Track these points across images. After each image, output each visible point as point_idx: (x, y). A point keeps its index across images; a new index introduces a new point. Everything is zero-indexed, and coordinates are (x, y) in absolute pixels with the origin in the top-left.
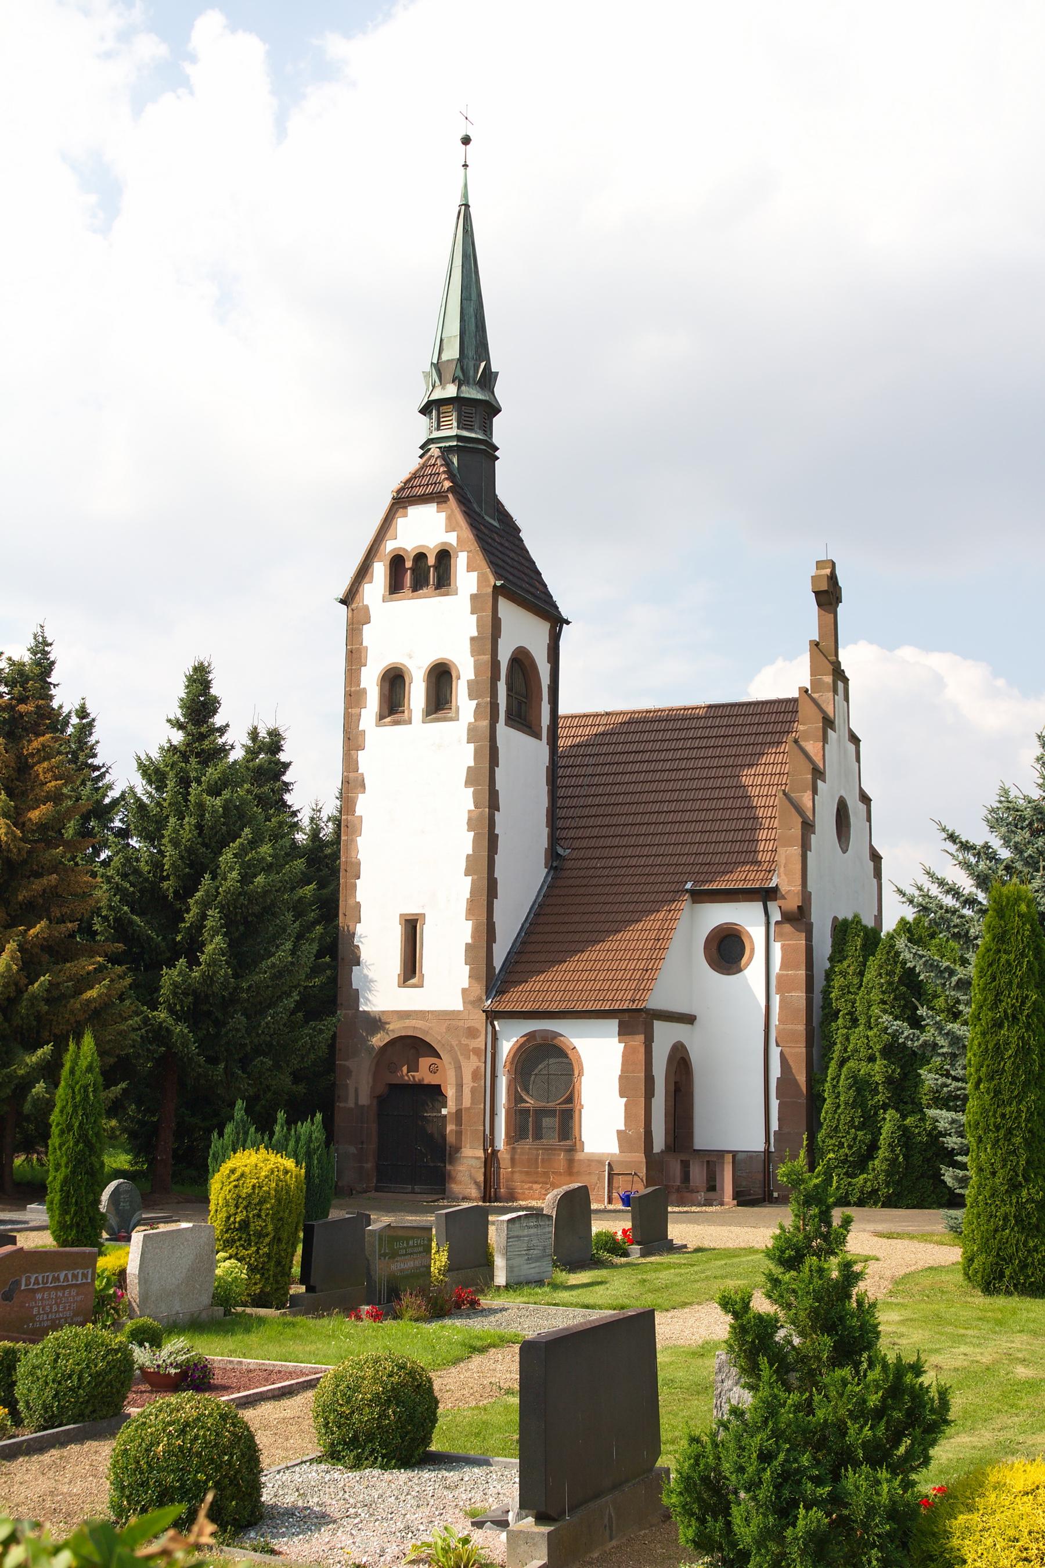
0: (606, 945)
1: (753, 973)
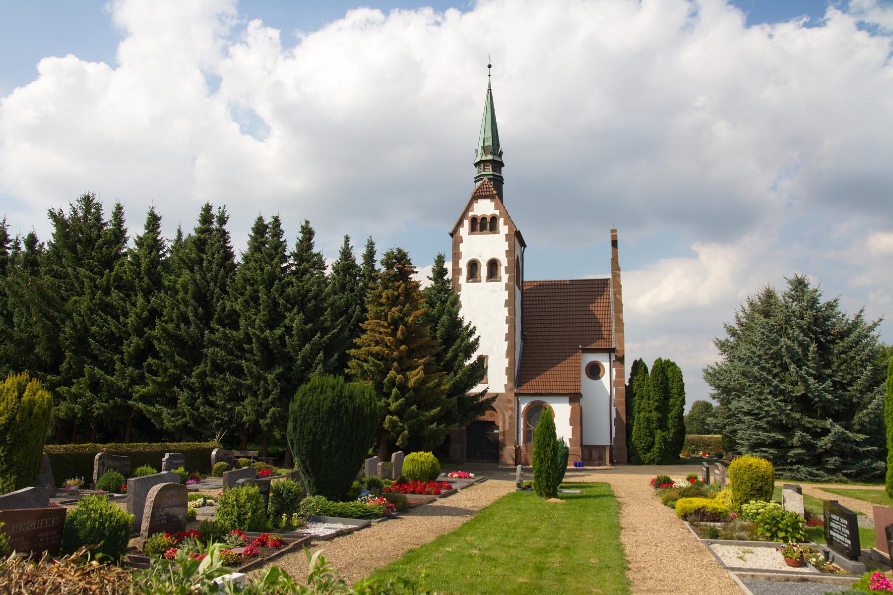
0: (555, 369)
1: (605, 380)
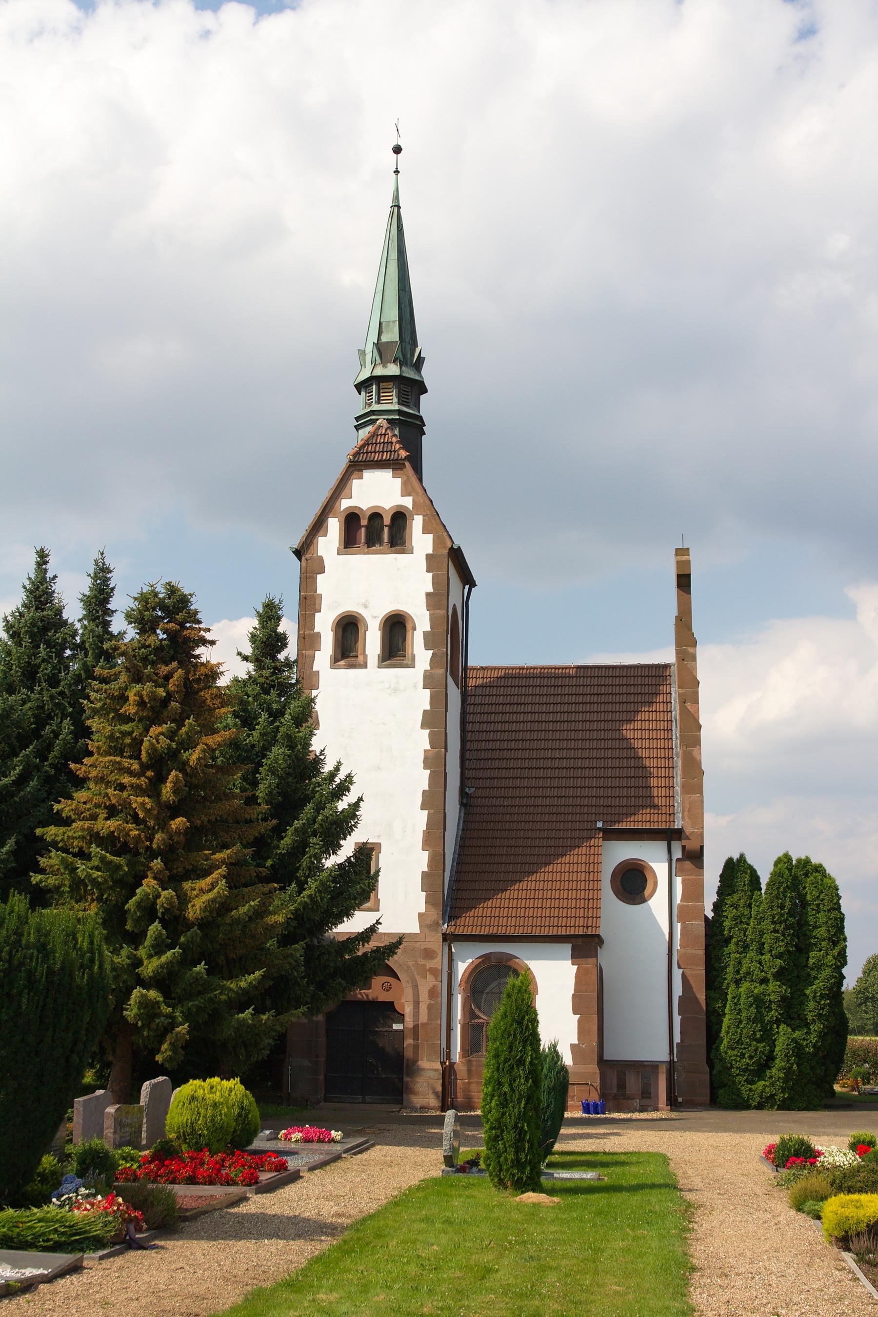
0: (540, 876)
1: (658, 904)
